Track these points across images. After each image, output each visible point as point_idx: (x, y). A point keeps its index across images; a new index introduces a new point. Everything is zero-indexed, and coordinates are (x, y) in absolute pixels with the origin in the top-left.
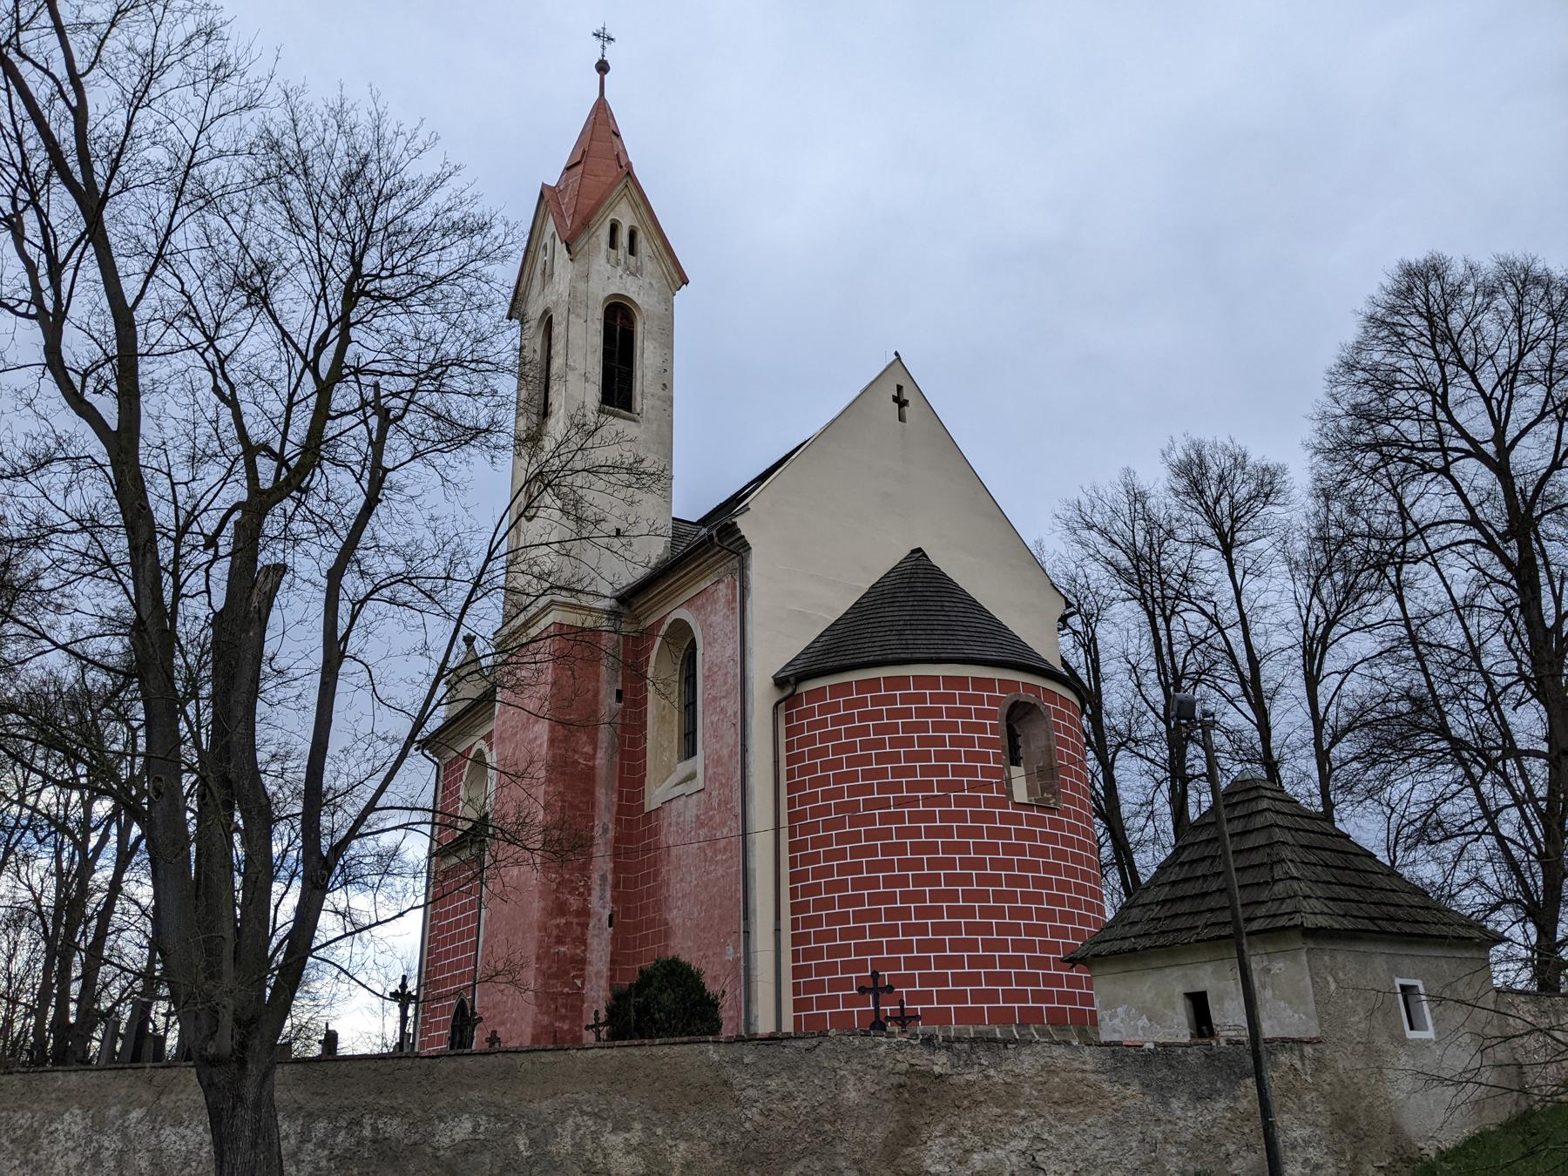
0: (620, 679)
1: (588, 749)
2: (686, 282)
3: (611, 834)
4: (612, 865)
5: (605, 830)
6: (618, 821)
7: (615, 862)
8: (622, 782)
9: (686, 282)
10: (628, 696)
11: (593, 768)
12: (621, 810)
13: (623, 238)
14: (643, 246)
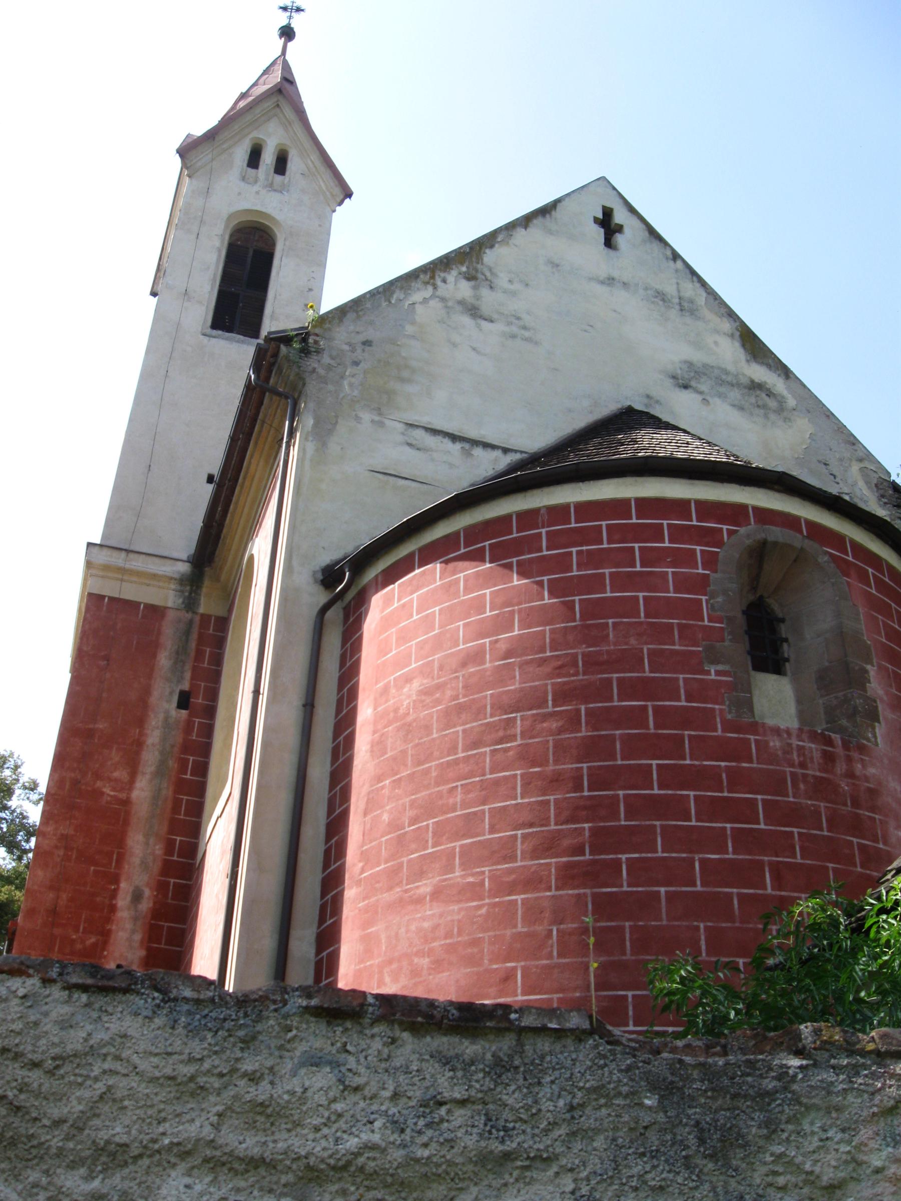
0: (188, 675)
1: (120, 774)
2: (349, 194)
3: (146, 905)
4: (143, 953)
5: (137, 897)
6: (161, 887)
7: (149, 949)
8: (174, 826)
9: (349, 194)
10: (199, 700)
11: (126, 803)
12: (167, 868)
13: (268, 158)
14: (294, 164)
